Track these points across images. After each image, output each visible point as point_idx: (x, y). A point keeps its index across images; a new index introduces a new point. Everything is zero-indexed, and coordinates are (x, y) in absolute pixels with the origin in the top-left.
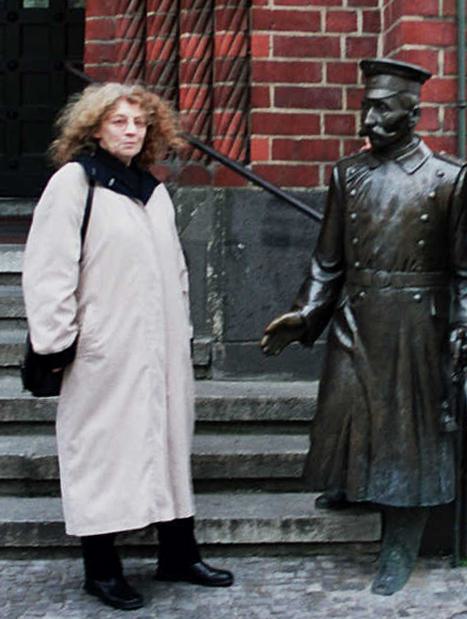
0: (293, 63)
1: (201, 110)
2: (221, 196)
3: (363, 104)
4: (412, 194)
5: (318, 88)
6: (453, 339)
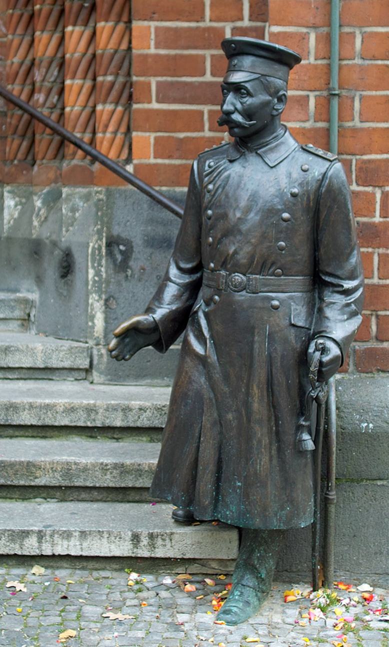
0: (175, 56)
1: (85, 107)
2: (101, 197)
5: (201, 83)
6: (311, 350)
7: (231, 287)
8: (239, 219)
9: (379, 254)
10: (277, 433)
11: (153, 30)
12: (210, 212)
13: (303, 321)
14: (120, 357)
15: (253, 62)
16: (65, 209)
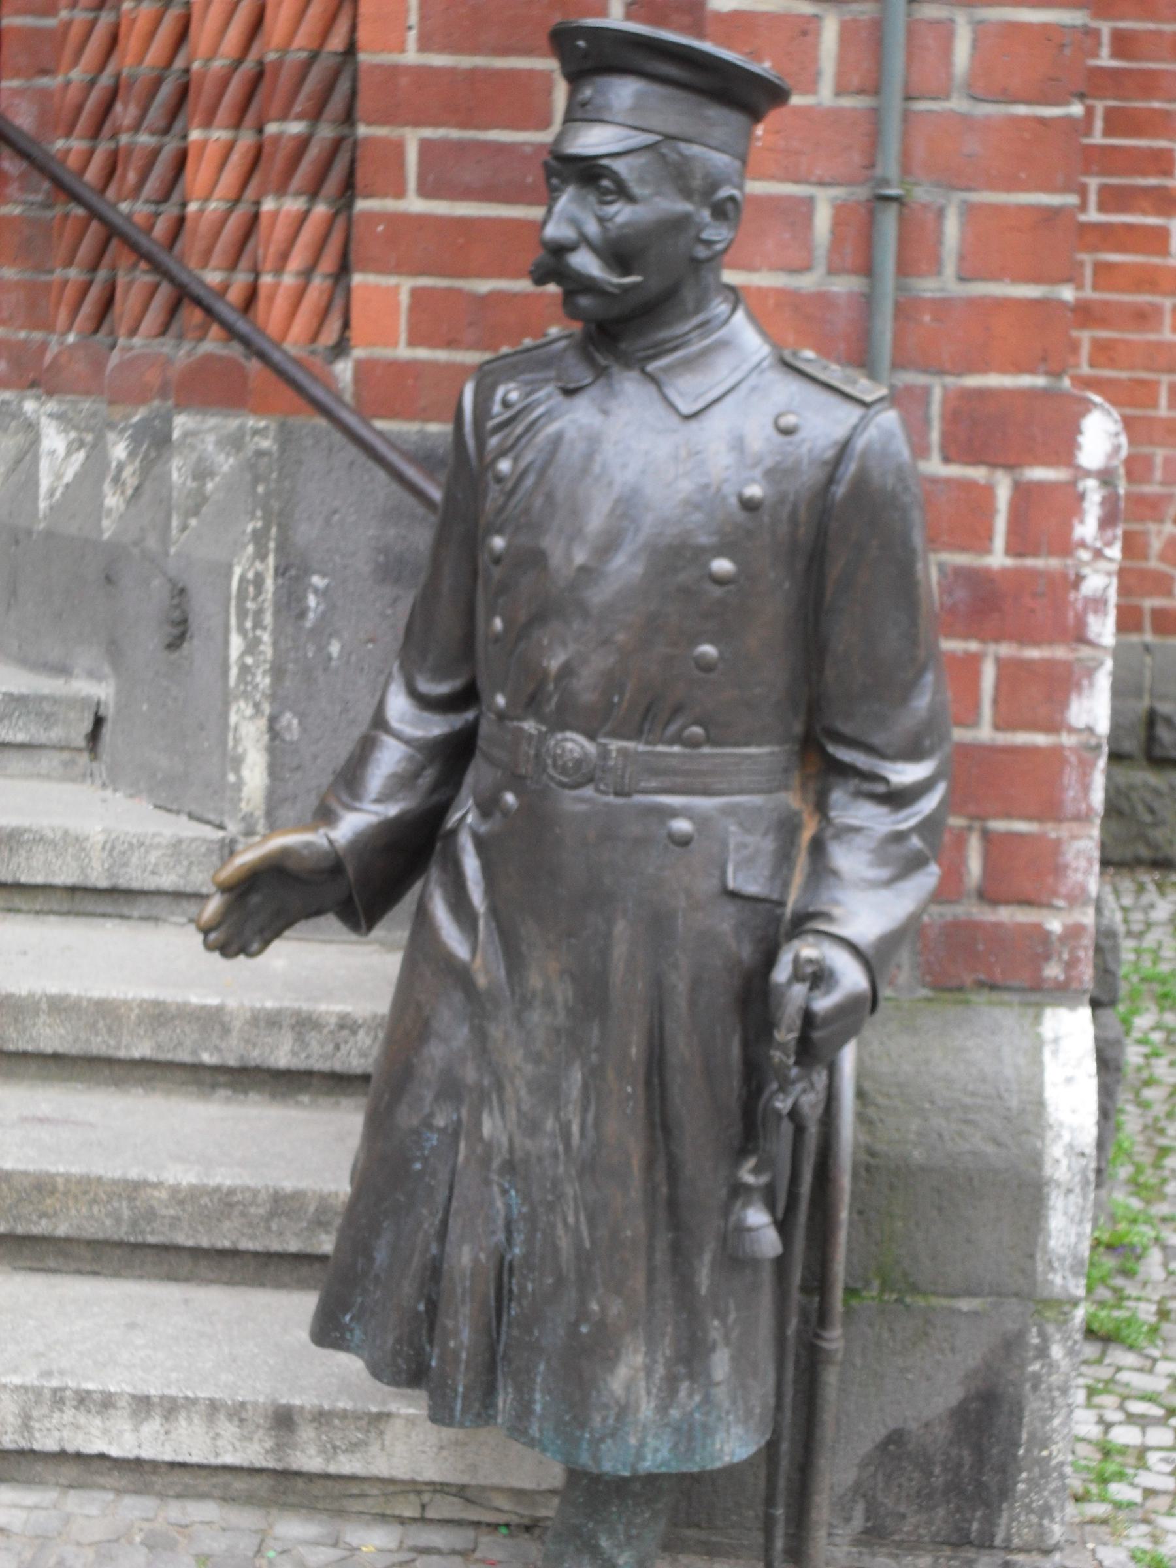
0: (473, 72)
1: (237, 200)
2: (266, 444)
3: (549, 172)
4: (686, 487)
7: (551, 771)
8: (583, 569)
10: (673, 1205)
12: (498, 542)
15: (639, 96)
16: (180, 469)
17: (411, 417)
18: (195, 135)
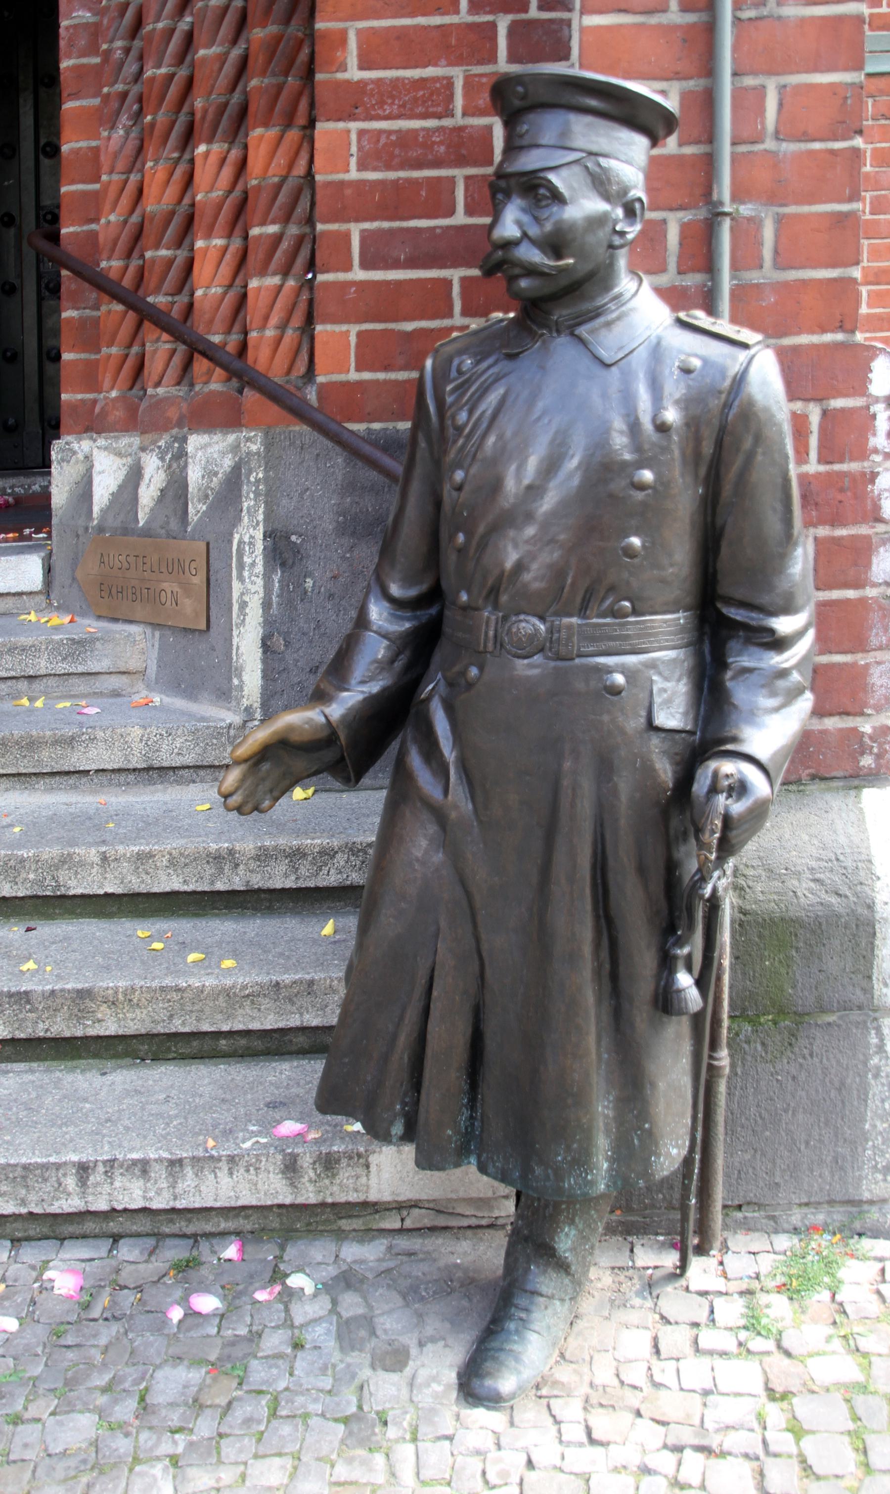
1: (230, 286)
5: (449, 228)
9: (816, 539)
11: (354, 137)
13: (678, 716)
14: (249, 806)
17: (361, 420)
18: (199, 244)
